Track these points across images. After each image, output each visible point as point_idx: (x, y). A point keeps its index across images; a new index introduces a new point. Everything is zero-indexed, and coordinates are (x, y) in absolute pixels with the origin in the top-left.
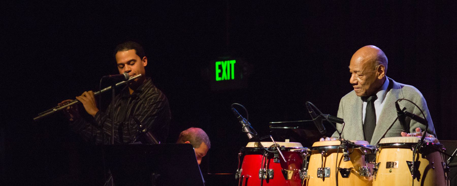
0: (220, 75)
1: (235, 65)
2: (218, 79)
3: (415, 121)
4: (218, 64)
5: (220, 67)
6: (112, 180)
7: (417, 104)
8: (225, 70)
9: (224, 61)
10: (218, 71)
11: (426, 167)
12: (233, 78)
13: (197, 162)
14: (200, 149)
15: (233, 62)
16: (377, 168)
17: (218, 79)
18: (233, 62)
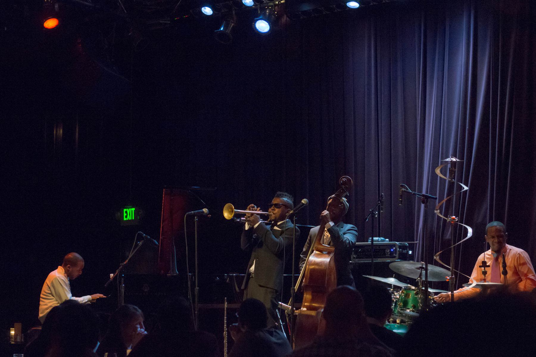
0: (126, 217)
2: (125, 219)
4: (125, 210)
5: (126, 212)
8: (129, 214)
10: (125, 214)
14: (58, 275)
15: (133, 209)
17: (125, 219)
18: (133, 209)
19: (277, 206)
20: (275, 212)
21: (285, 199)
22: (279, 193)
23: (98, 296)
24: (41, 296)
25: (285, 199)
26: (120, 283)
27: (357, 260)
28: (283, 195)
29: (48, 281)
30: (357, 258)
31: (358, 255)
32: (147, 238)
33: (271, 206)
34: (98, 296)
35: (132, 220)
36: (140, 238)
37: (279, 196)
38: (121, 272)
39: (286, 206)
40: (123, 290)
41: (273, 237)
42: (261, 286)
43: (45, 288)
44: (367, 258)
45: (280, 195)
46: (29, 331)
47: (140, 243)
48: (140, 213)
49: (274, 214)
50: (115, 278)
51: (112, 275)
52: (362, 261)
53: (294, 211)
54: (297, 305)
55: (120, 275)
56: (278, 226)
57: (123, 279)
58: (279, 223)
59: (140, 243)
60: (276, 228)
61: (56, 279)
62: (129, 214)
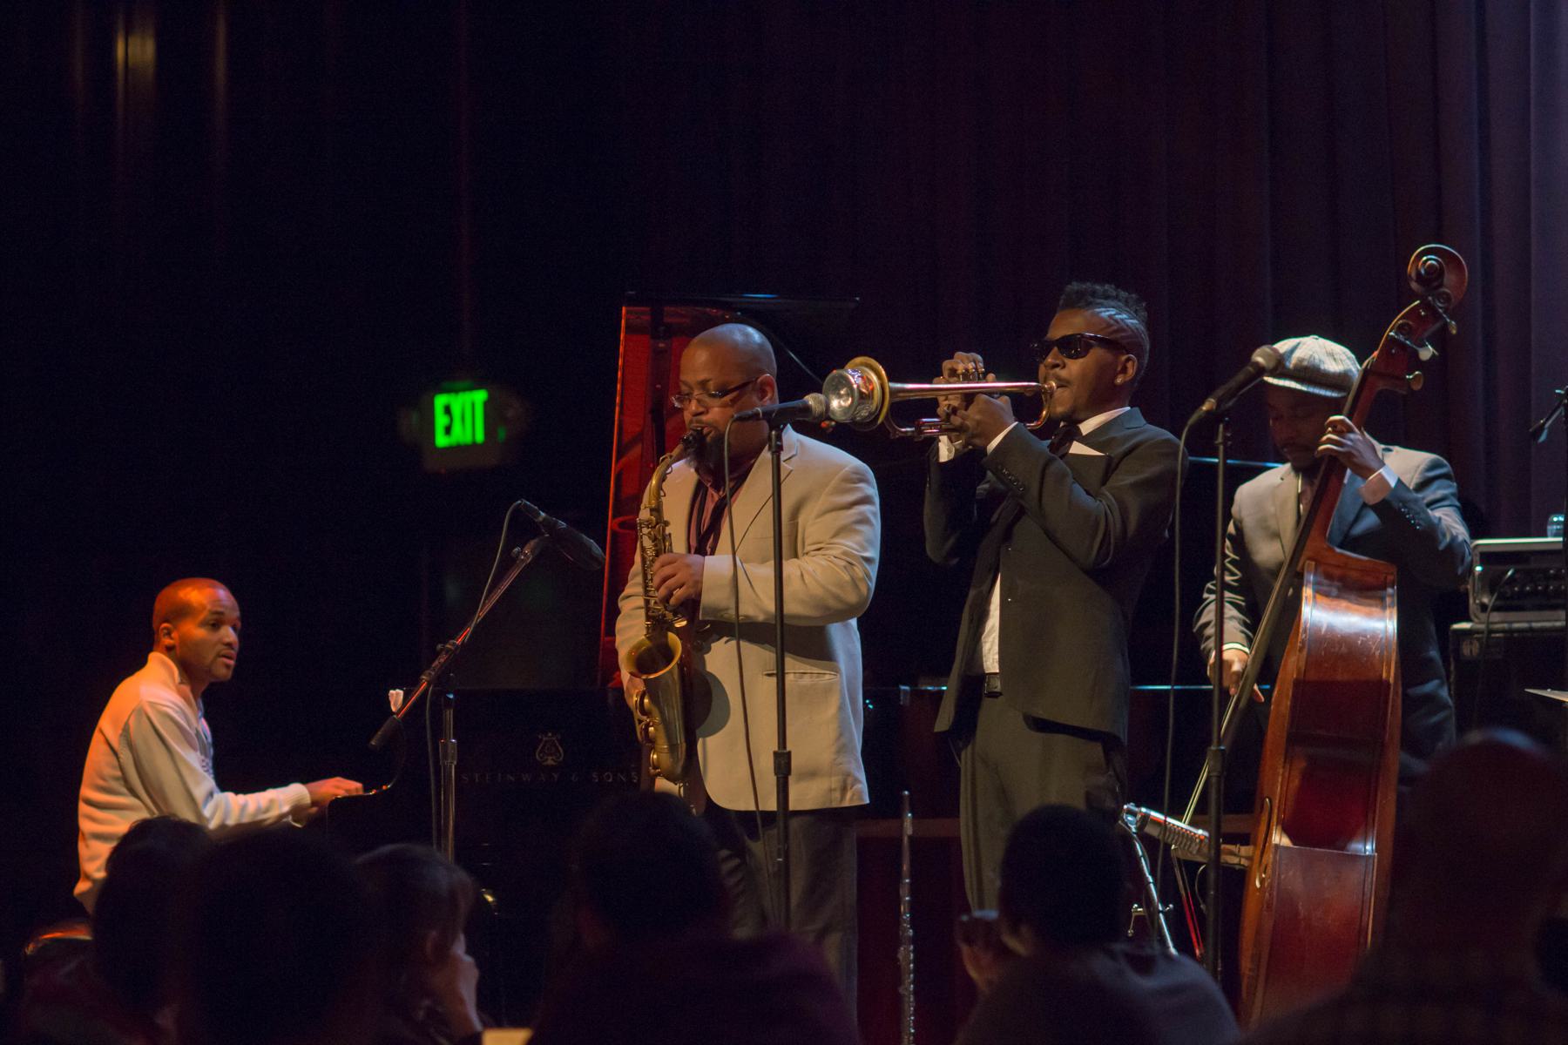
0: (448, 430)
1: (486, 404)
2: (441, 440)
3: (223, 669)
4: (440, 401)
5: (448, 410)
6: (596, 549)
7: (790, 567)
8: (460, 417)
9: (456, 391)
10: (441, 420)
11: (979, 733)
12: (480, 437)
13: (1377, 850)
14: (153, 693)
15: (480, 396)
16: (1406, 789)
17: (441, 440)
18: (480, 396)
19: (1072, 346)
20: (1063, 373)
21: (1106, 313)
22: (1075, 286)
23: (339, 787)
24: (86, 792)
25: (1106, 313)
26: (438, 732)
27: (1496, 617)
28: (1094, 294)
29: (108, 725)
30: (1496, 609)
31: (1501, 597)
32: (551, 527)
33: (1046, 352)
34: (339, 787)
35: (474, 445)
36: (524, 529)
37: (1082, 301)
38: (440, 682)
39: (1114, 342)
40: (452, 765)
41: (1078, 490)
42: (1042, 725)
43: (97, 757)
44: (1540, 608)
45: (1081, 295)
46: (30, 949)
47: (526, 553)
48: (510, 414)
49: (1063, 384)
50: (414, 713)
51: (396, 696)
52: (1521, 622)
53: (1219, 402)
54: (1233, 824)
55: (439, 694)
56: (1086, 440)
57: (449, 715)
58: (1087, 427)
59: (526, 553)
60: (1077, 448)
61: (140, 712)
62: (460, 417)
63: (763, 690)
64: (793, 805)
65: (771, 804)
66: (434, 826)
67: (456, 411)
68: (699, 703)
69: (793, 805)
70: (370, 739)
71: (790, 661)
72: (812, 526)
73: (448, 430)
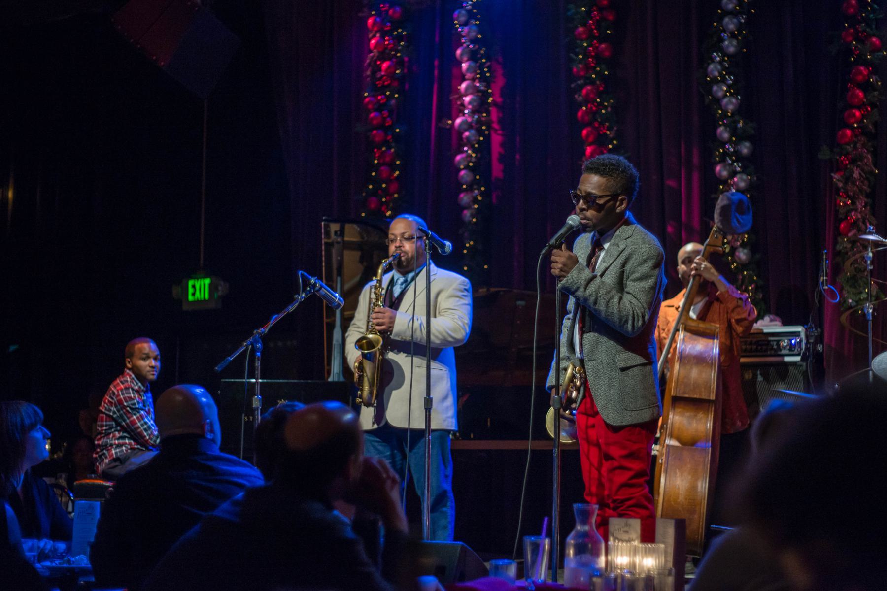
0: (194, 294)
1: (210, 285)
2: (191, 298)
5: (194, 286)
8: (199, 289)
10: (191, 290)
15: (207, 281)
18: (207, 281)
26: (564, 312)
63: (420, 372)
64: (433, 427)
65: (418, 423)
66: (545, 526)
67: (197, 287)
68: (387, 376)
69: (433, 427)
70: (216, 365)
71: (433, 365)
72: (444, 302)
73: (194, 294)
